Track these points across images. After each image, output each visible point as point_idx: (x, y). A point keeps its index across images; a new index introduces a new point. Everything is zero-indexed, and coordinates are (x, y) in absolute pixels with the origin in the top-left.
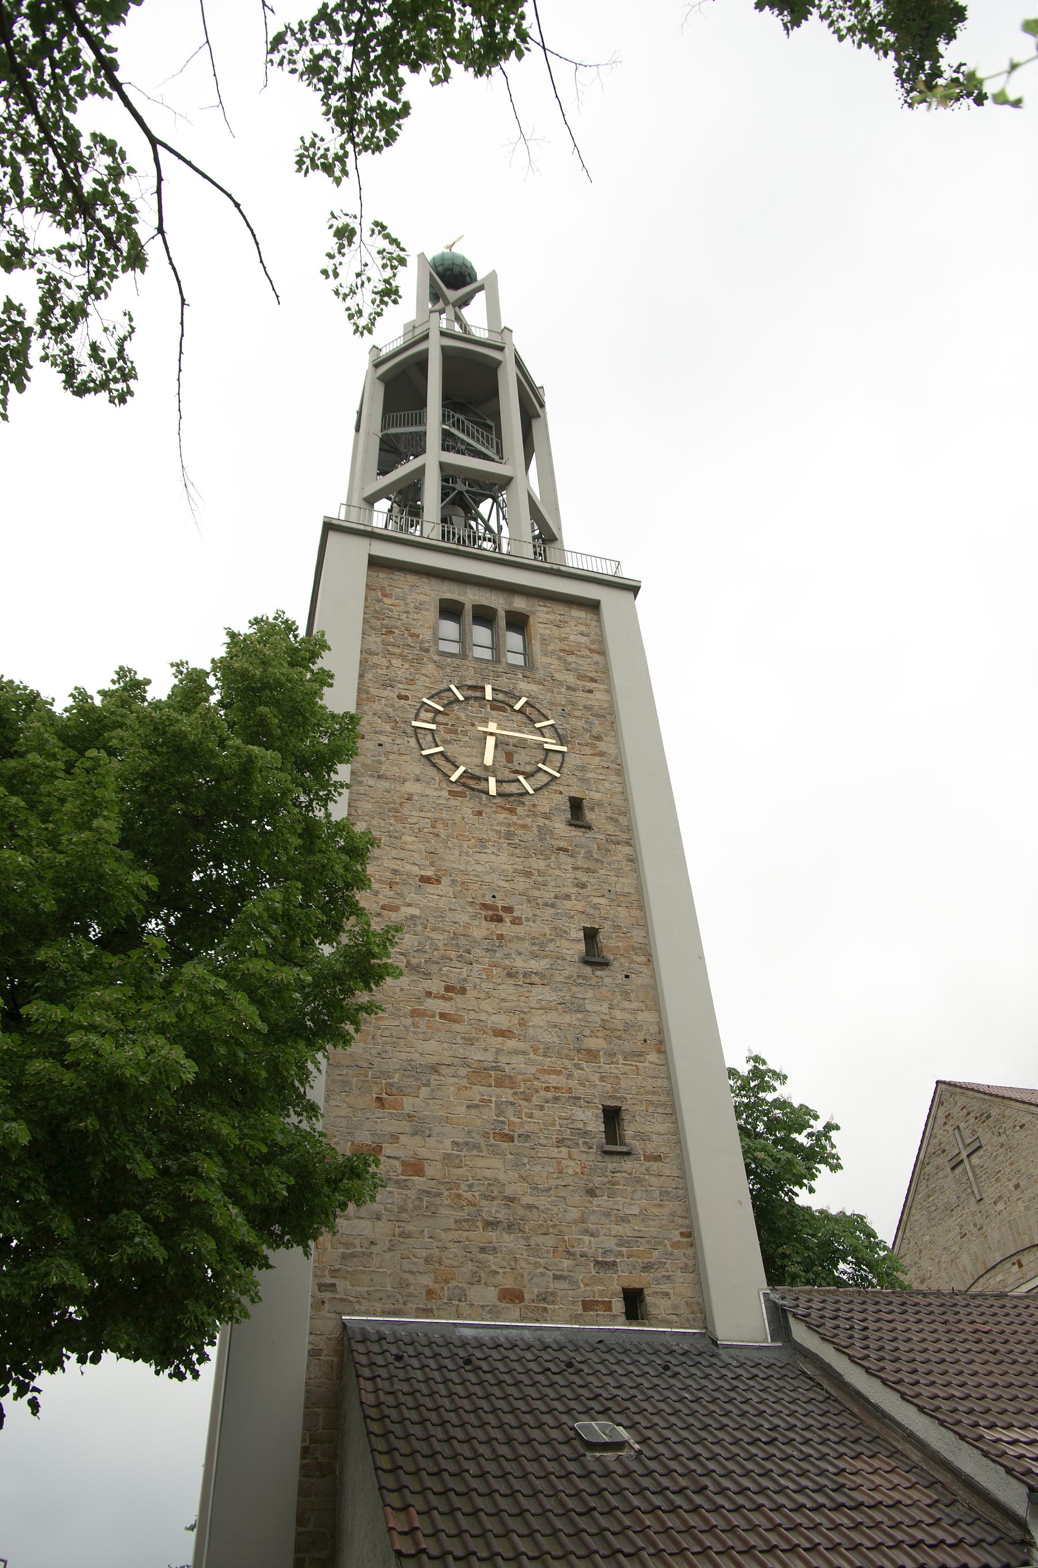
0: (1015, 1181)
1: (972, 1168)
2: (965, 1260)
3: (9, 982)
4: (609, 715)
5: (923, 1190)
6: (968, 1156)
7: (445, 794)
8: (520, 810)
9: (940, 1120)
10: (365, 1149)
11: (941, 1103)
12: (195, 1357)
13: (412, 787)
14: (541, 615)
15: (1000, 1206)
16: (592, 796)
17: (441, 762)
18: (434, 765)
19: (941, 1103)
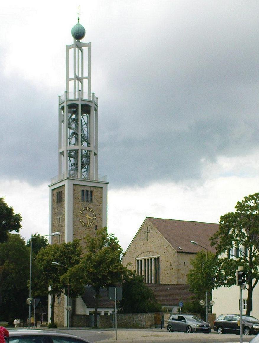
0: (153, 241)
1: (148, 235)
2: (142, 249)
3: (51, 273)
4: (101, 210)
5: (139, 234)
6: (148, 233)
7: (82, 227)
8: (90, 228)
9: (145, 224)
10: (63, 206)
11: (146, 221)
12: (58, 280)
13: (78, 226)
14: (95, 190)
15: (150, 243)
16: (98, 225)
17: (82, 222)
18: (81, 222)
19: (146, 221)
